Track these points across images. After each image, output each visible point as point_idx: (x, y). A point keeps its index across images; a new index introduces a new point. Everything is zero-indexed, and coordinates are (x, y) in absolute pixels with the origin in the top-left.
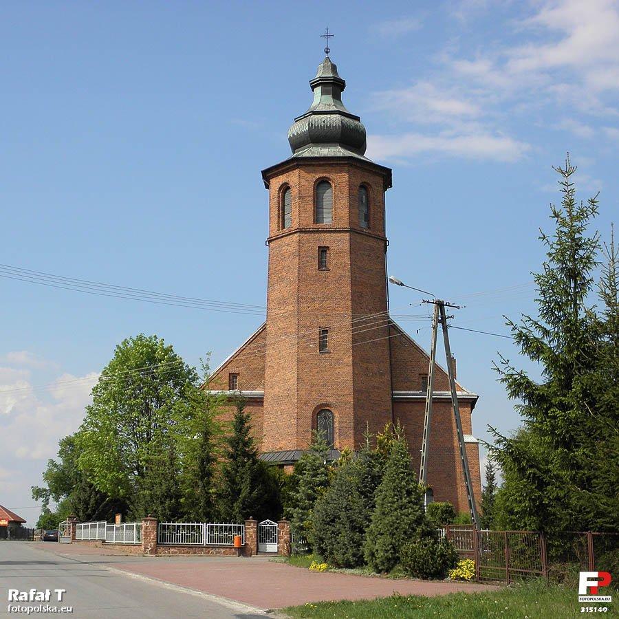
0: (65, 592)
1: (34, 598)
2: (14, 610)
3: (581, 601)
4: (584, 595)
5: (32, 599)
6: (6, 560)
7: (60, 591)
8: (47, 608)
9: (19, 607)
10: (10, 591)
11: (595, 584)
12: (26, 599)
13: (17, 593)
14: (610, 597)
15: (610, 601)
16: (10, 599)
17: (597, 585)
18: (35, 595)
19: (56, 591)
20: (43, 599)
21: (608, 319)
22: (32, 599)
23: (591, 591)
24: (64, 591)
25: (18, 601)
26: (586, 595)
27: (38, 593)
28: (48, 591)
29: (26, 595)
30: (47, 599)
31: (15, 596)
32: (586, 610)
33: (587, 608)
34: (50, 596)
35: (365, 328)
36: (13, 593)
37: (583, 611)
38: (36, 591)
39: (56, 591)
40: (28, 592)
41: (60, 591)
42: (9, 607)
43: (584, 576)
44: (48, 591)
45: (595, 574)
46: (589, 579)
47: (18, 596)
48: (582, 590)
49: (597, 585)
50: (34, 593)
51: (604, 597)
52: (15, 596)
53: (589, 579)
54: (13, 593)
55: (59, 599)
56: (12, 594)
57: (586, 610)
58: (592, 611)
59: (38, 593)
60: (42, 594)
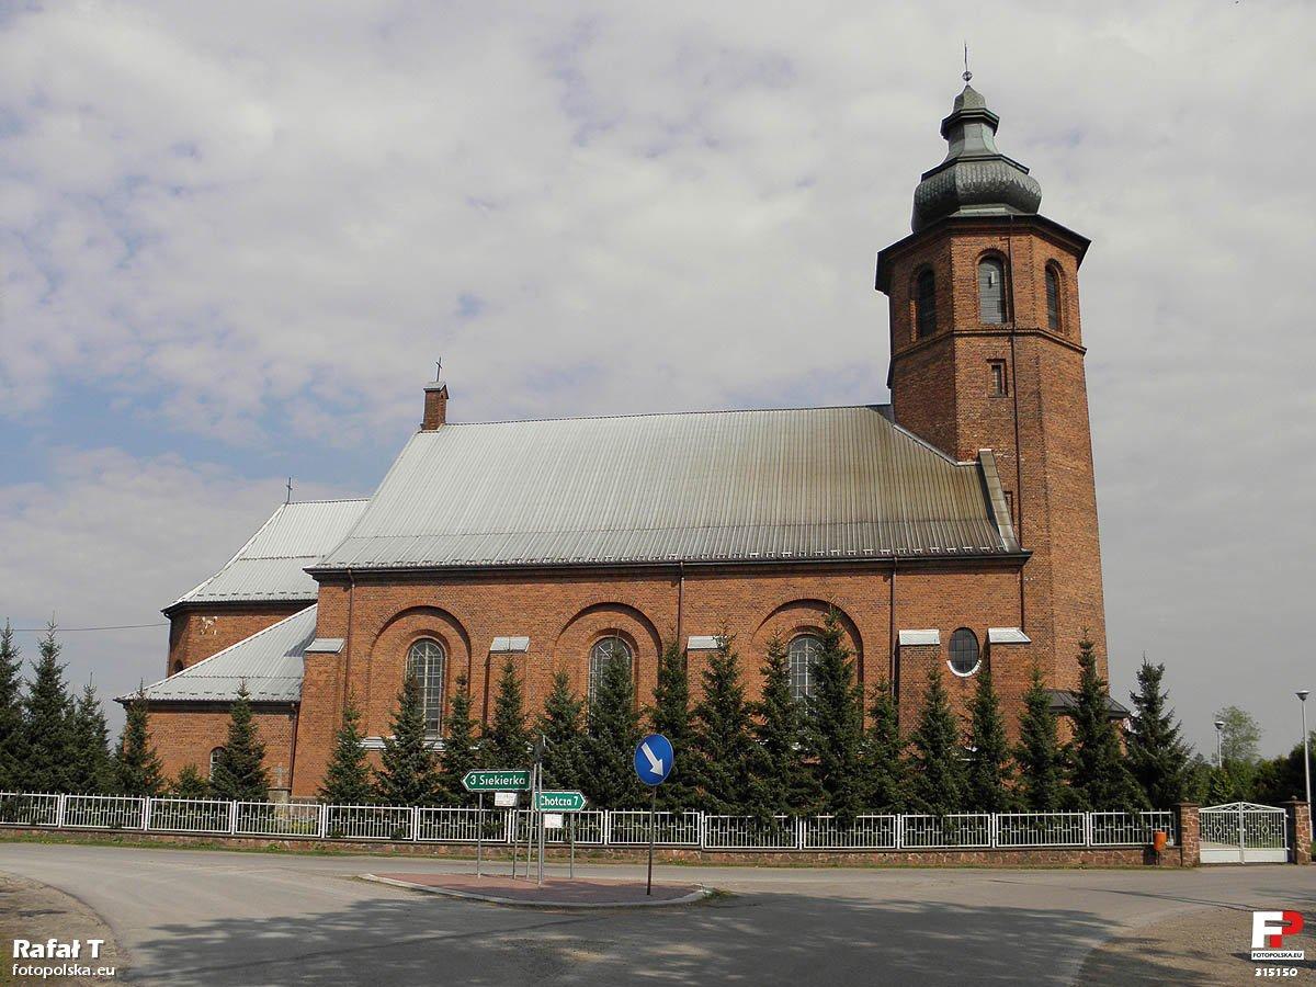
0: (104, 944)
1: (54, 954)
2: (23, 971)
3: (1256, 958)
4: (1260, 949)
5: (50, 955)
6: (710, 584)
7: (95, 943)
8: (75, 970)
9: (30, 968)
10: (17, 943)
11: (1278, 931)
12: (42, 955)
13: (27, 944)
14: (1302, 952)
15: (1302, 958)
16: (16, 955)
17: (1280, 933)
18: (56, 949)
19: (89, 942)
20: (68, 956)
21: (575, 700)
22: (50, 955)
23: (1273, 942)
24: (102, 942)
25: (30, 958)
26: (1263, 949)
27: (34, 946)
28: (76, 942)
29: (41, 948)
30: (75, 955)
31: (24, 950)
32: (1263, 972)
33: (1265, 970)
34: (80, 950)
35: (590, 548)
36: (21, 945)
37: (1259, 974)
38: (58, 943)
39: (89, 942)
40: (45, 945)
41: (95, 943)
42: (15, 968)
43: (1259, 918)
44: (76, 942)
45: (1278, 916)
46: (1269, 923)
47: (28, 950)
48: (1258, 941)
49: (1280, 933)
50: (55, 946)
51: (1293, 953)
52: (24, 950)
53: (1269, 923)
54: (21, 945)
55: (95, 955)
56: (20, 947)
57: (1263, 972)
58: (1273, 974)
59: (60, 946)
60: (67, 947)
